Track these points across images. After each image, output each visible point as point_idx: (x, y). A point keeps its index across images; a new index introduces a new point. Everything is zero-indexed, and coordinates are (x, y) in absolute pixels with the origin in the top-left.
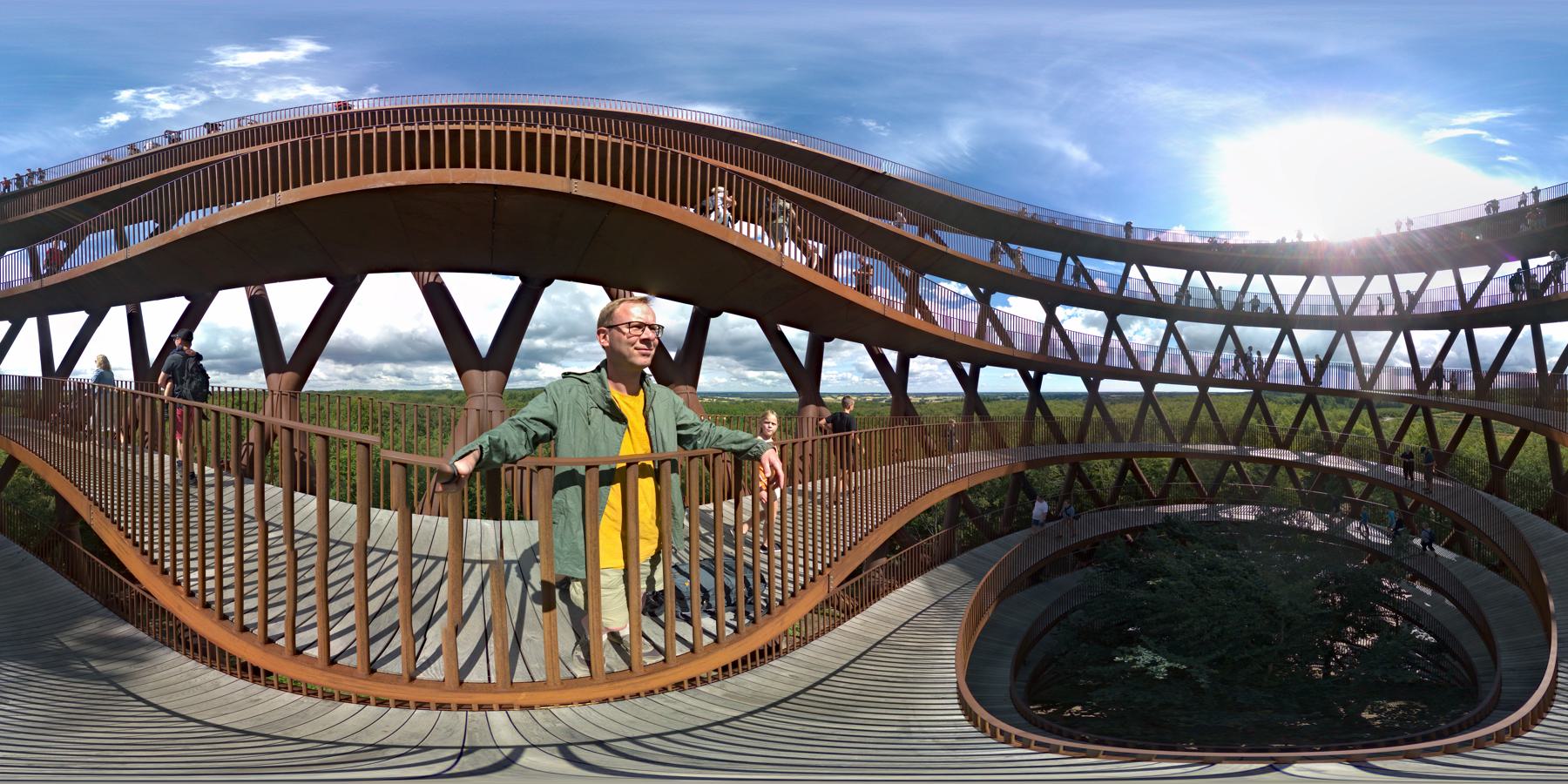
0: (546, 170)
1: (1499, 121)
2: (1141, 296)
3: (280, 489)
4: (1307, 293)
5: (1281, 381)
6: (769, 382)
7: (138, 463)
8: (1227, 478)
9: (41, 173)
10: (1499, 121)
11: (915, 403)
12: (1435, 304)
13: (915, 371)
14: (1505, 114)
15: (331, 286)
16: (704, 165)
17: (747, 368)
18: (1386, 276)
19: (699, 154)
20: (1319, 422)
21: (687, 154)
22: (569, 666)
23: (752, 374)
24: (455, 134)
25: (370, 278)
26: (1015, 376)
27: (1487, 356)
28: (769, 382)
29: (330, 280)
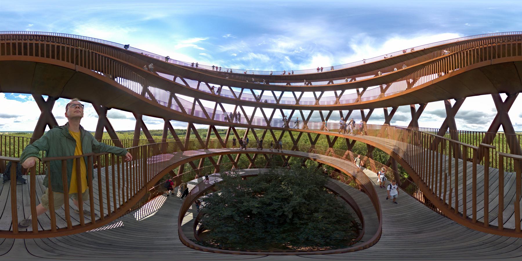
0: (26, 54)
1: (200, 42)
2: (230, 97)
3: (472, 163)
4: (263, 95)
5: (256, 124)
6: (475, 128)
7: (432, 154)
8: (368, 160)
9: (322, 69)
10: (200, 42)
11: (176, 130)
12: (347, 100)
13: (96, 118)
14: (205, 39)
15: (456, 101)
16: (99, 55)
17: (467, 122)
18: (490, 96)
19: (98, 51)
20: (334, 140)
21: (93, 51)
22: (35, 242)
23: (470, 125)
24: (31, 44)
25: (467, 98)
26: (163, 120)
27: (268, 116)
28: (475, 128)
29: (455, 100)
